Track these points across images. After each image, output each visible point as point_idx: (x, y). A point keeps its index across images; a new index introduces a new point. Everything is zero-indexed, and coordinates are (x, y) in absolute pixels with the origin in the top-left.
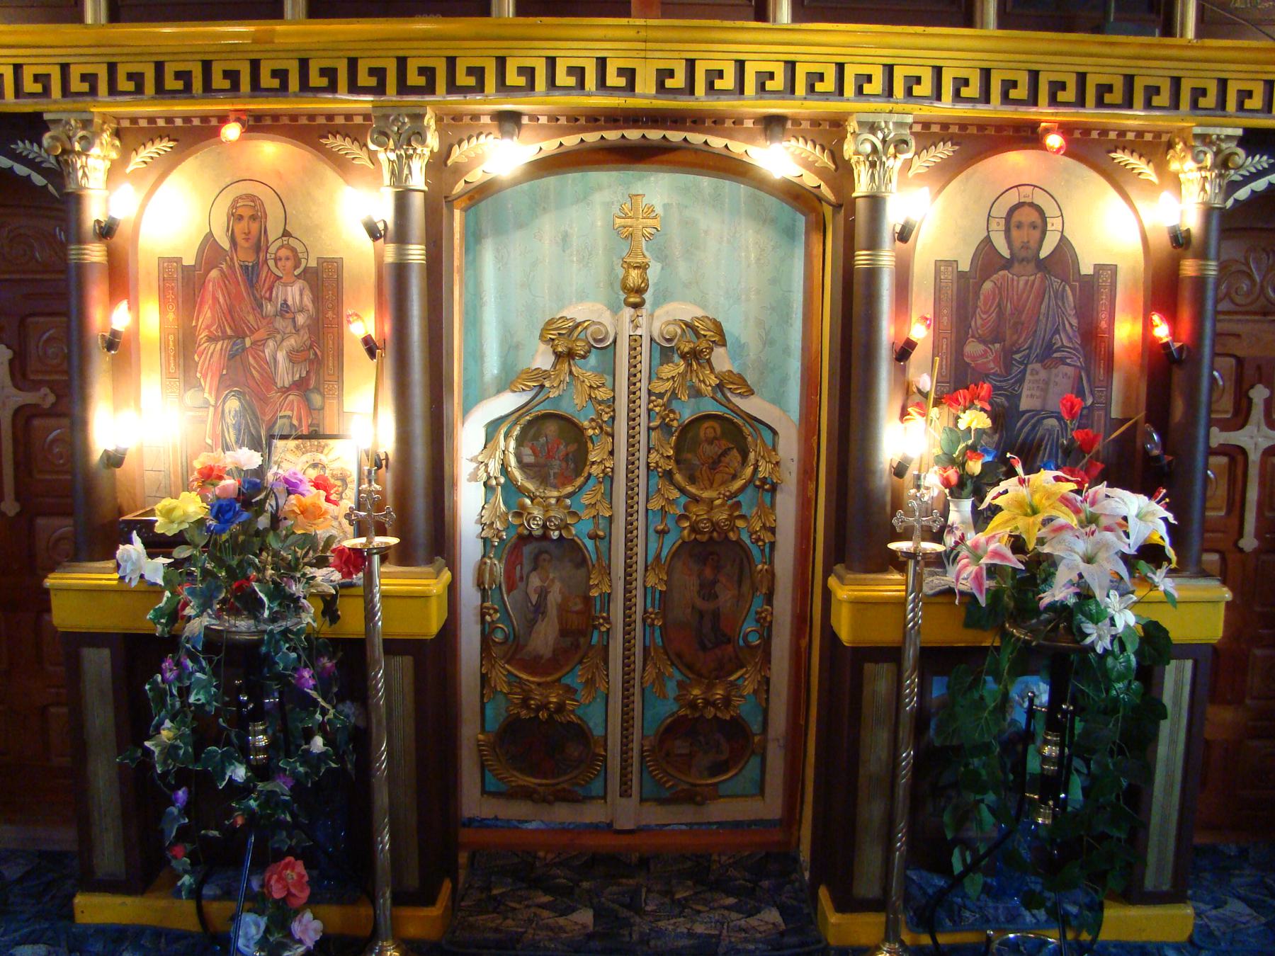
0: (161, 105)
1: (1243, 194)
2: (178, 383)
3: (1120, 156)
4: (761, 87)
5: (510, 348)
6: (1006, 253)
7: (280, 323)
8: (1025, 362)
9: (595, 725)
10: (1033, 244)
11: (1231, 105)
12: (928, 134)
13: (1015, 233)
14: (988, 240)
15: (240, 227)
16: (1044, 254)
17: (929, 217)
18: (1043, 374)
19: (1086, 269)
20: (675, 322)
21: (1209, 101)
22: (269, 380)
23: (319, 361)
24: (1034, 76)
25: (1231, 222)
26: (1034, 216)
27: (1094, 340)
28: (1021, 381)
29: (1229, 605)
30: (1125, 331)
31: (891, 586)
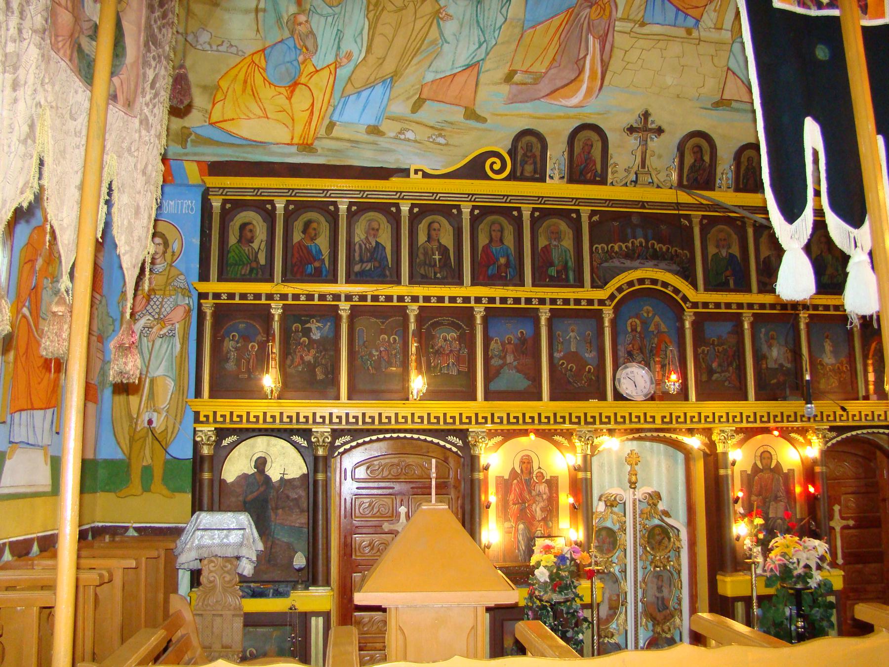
1: (829, 444)
3: (793, 435)
4: (691, 420)
7: (537, 498)
11: (825, 419)
12: (738, 431)
14: (755, 464)
15: (524, 466)
16: (772, 467)
17: (739, 457)
18: (775, 505)
19: (785, 471)
21: (818, 419)
22: (534, 518)
23: (551, 509)
24: (769, 414)
25: (828, 453)
26: (768, 455)
27: (789, 493)
28: (769, 508)
29: (844, 576)
30: (798, 489)
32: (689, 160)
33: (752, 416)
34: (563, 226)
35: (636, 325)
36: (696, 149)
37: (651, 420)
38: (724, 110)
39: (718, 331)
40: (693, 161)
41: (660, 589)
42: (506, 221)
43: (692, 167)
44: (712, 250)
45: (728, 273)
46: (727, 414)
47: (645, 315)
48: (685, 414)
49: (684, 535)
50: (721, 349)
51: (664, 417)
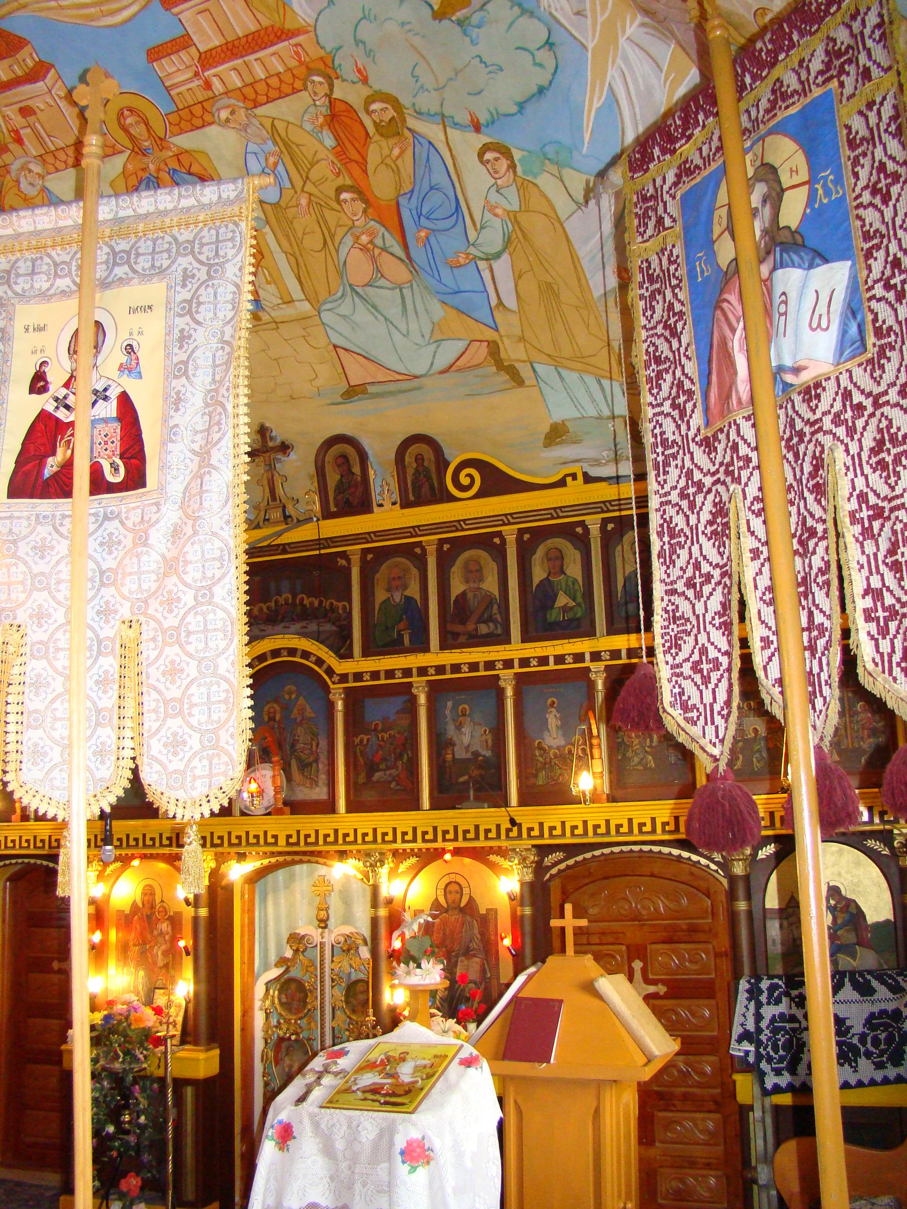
2: (122, 963)
5: (279, 947)
6: (445, 905)
7: (160, 939)
8: (457, 956)
10: (457, 900)
13: (449, 896)
15: (146, 898)
18: (466, 962)
19: (483, 911)
20: (342, 935)
22: (155, 963)
24: (435, 829)
26: (457, 888)
32: (333, 478)
33: (537, 827)
34: (482, 555)
35: (275, 712)
36: (340, 461)
37: (273, 841)
38: (360, 400)
39: (375, 711)
40: (338, 477)
42: (569, 545)
43: (339, 489)
44: (380, 595)
45: (401, 626)
46: (375, 830)
47: (287, 697)
48: (317, 832)
50: (386, 736)
51: (289, 837)
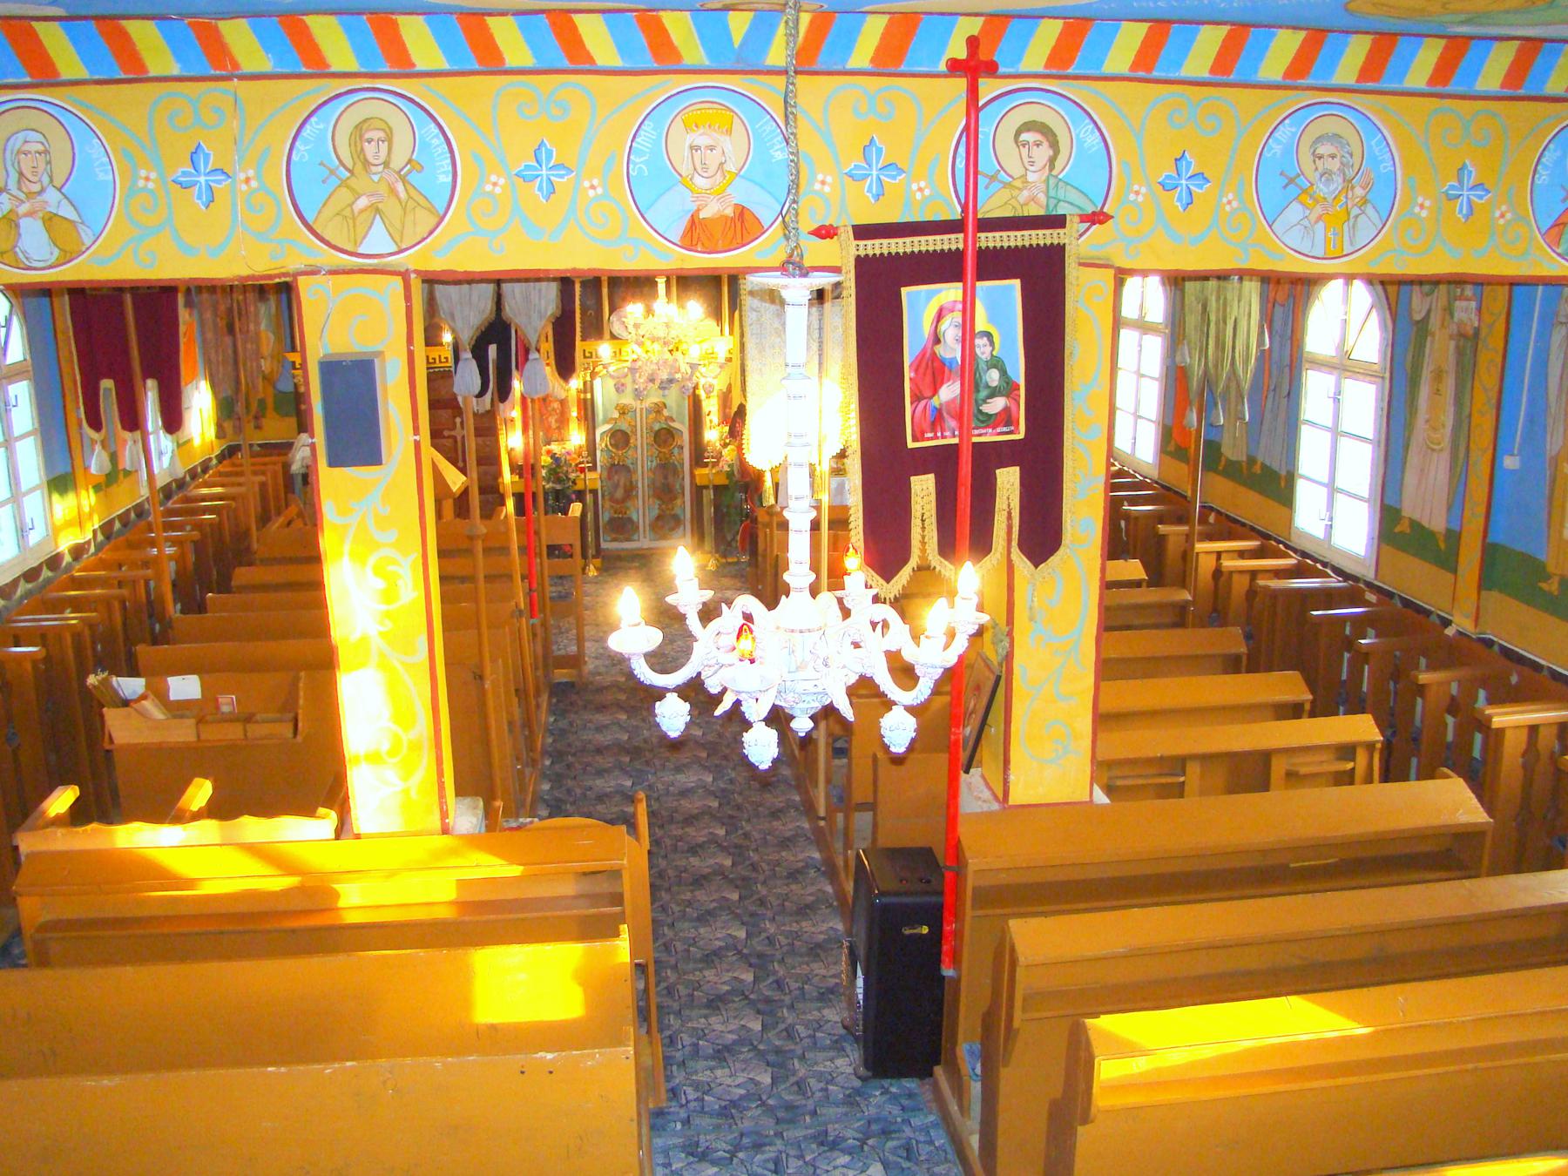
0: (1555, 709)
5: (605, 411)
9: (635, 518)
23: (563, 421)
31: (705, 471)
41: (666, 478)
49: (686, 436)
